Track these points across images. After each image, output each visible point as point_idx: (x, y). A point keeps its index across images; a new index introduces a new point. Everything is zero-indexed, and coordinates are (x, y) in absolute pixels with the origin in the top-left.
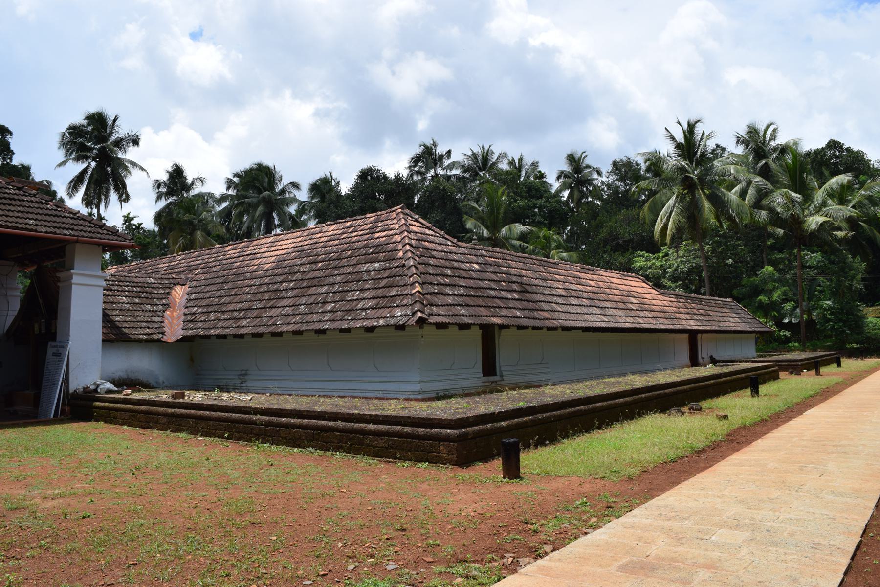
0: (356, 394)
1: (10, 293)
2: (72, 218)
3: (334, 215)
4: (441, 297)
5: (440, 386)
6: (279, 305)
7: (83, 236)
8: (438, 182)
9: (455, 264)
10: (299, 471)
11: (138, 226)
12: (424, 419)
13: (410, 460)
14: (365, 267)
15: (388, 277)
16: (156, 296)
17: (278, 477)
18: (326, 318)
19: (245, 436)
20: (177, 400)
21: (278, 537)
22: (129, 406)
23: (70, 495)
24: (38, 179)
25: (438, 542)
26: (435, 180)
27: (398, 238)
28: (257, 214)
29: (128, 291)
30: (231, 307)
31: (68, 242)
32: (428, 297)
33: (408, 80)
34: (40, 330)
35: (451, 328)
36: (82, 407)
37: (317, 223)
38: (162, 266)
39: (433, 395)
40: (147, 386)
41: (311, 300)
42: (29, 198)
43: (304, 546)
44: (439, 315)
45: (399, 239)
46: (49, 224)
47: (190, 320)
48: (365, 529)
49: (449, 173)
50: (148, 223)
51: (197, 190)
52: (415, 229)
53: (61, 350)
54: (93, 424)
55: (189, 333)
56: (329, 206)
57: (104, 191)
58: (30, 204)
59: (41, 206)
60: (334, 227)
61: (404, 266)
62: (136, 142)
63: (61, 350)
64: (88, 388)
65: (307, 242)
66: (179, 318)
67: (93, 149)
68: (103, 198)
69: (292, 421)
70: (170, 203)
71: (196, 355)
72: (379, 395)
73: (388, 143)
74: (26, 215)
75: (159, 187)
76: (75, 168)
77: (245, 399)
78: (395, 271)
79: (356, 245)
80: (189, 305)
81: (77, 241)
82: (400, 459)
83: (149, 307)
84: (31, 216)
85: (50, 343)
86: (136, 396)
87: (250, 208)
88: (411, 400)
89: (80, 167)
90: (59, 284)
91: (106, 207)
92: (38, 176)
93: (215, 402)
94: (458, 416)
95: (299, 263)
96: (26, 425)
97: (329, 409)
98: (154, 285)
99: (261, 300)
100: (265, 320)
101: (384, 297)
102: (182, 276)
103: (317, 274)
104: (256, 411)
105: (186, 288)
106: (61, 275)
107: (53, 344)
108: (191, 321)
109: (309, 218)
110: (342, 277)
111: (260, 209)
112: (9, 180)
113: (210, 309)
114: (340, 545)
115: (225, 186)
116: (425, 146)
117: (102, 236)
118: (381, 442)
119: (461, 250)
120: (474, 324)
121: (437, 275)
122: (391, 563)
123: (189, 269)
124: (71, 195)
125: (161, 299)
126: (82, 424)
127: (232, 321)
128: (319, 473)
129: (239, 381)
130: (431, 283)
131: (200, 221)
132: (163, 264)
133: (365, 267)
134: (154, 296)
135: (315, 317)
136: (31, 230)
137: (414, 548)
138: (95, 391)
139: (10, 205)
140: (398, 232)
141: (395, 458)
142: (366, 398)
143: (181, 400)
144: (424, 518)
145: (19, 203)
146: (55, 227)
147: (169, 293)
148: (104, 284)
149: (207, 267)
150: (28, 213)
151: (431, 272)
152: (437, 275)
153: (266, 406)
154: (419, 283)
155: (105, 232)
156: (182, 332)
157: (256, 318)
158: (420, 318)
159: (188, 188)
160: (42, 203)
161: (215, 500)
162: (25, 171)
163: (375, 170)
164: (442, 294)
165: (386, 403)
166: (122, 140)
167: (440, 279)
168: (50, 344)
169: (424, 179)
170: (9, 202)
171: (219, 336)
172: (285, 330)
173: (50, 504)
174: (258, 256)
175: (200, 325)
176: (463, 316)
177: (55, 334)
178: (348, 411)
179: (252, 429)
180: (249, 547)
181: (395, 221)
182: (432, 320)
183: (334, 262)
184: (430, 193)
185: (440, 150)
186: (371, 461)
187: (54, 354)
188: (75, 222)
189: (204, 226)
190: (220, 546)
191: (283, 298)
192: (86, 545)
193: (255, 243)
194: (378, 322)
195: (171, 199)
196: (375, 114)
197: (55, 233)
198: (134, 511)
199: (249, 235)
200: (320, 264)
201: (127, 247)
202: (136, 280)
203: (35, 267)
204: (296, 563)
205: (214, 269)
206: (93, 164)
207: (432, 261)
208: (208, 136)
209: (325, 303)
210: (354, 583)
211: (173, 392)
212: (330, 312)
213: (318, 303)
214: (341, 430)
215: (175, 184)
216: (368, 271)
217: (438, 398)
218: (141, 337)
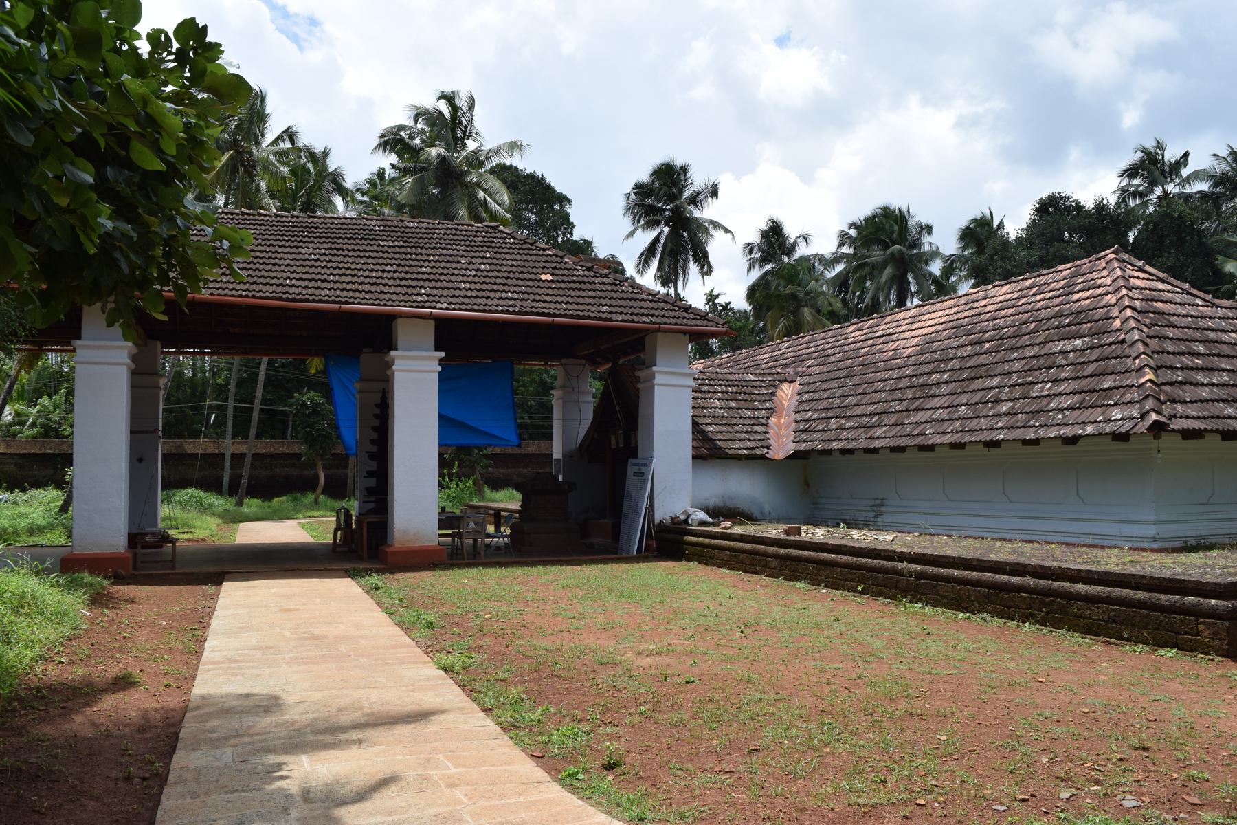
0: (1050, 539)
1: (582, 398)
3: (999, 271)
4: (1188, 388)
5: (1190, 530)
6: (928, 406)
8: (1168, 205)
9: (1212, 335)
10: (970, 646)
11: (726, 307)
12: (1169, 580)
13: (1146, 643)
14: (1059, 346)
15: (1097, 360)
16: (758, 398)
17: (940, 652)
18: (1000, 424)
19: (887, 591)
20: (792, 538)
21: (950, 737)
23: (668, 652)
24: (601, 256)
25: (1207, 776)
26: (1164, 203)
27: (1112, 299)
28: (884, 278)
30: (859, 411)
32: (1168, 388)
33: (1096, 55)
34: (617, 443)
35: (1208, 437)
36: (670, 542)
37: (975, 286)
39: (1178, 544)
40: (750, 518)
41: (977, 398)
42: (600, 280)
43: (989, 754)
44: (1187, 417)
45: (1113, 301)
46: (625, 311)
47: (804, 428)
48: (1082, 741)
49: (1188, 190)
50: (740, 302)
51: (802, 251)
52: (1138, 283)
53: (643, 469)
54: (684, 564)
55: (803, 446)
56: (992, 259)
57: (680, 264)
58: (602, 287)
60: (1005, 289)
61: (1123, 341)
62: (714, 192)
63: (643, 469)
65: (966, 314)
66: (788, 426)
67: (664, 210)
68: (680, 272)
69: (956, 573)
70: (766, 273)
71: (811, 476)
72: (1088, 542)
73: (1074, 153)
74: (598, 301)
76: (645, 238)
77: (884, 539)
78: (1108, 350)
79: (1043, 314)
80: (801, 408)
81: (659, 330)
82: (1128, 640)
83: (749, 413)
84: (604, 302)
86: (737, 530)
87: (873, 271)
88: (1144, 550)
89: (652, 234)
90: (639, 386)
91: (684, 283)
92: (601, 252)
93: (843, 542)
94: (1230, 579)
95: (955, 344)
96: (606, 561)
97: (1012, 558)
99: (901, 400)
100: (909, 428)
101: (1093, 391)
102: (790, 370)
103: (983, 359)
104: (902, 557)
105: (796, 387)
106: (641, 374)
108: (805, 431)
109: (960, 280)
110: (1023, 362)
111: (888, 271)
112: (576, 260)
113: (830, 414)
114: (1045, 760)
116: (1144, 151)
117: (689, 322)
118: (1097, 613)
119: (1221, 312)
120: (1211, 431)
121: (1180, 354)
122: (1129, 797)
123: (799, 360)
124: (640, 272)
126: (671, 564)
127: (861, 430)
128: (1000, 651)
129: (872, 514)
130: (1171, 368)
131: (807, 294)
132: (764, 354)
133: (1059, 346)
134: (753, 398)
135: (984, 424)
136: (606, 319)
137: (1166, 779)
138: (686, 521)
140: (1110, 289)
141: (1121, 638)
142: (1067, 544)
143: (797, 538)
144: (1179, 734)
145: (589, 286)
146: (632, 314)
147: (773, 394)
148: (694, 384)
149: (822, 357)
151: (1171, 349)
152: (1180, 354)
153: (916, 550)
154: (1151, 368)
155: (692, 316)
156: (793, 446)
157: (895, 425)
158: (1156, 422)
159: (790, 250)
161: (854, 676)
162: (587, 245)
163: (1061, 197)
164: (1191, 384)
165: (1101, 553)
166: (698, 194)
167: (1186, 360)
168: (631, 461)
169: (1145, 204)
171: (843, 452)
172: (938, 441)
173: (645, 662)
174: (894, 337)
175: (817, 436)
176: (1230, 417)
177: (636, 448)
178: (1042, 563)
179: (897, 581)
180: (907, 745)
181: (1105, 273)
182: (1177, 424)
183: (1010, 340)
184: (1155, 224)
185: (1171, 154)
186: (1081, 641)
187: (636, 474)
188: (655, 305)
189: (811, 299)
190: (869, 741)
191: (933, 396)
192: (693, 717)
193: (888, 319)
194: (1084, 429)
195: (768, 267)
196: (1053, 113)
197: (633, 321)
198: (749, 680)
199: (874, 309)
200: (987, 345)
201: (713, 335)
202: (731, 377)
203: (609, 365)
204: (979, 777)
205: (833, 358)
206: (666, 230)
207: (1170, 333)
208: (807, 176)
209: (997, 401)
210: (1071, 818)
211: (785, 526)
212: (1007, 414)
213: (987, 402)
214: (1033, 591)
216: (1064, 353)
217: (1187, 549)
218: (740, 452)
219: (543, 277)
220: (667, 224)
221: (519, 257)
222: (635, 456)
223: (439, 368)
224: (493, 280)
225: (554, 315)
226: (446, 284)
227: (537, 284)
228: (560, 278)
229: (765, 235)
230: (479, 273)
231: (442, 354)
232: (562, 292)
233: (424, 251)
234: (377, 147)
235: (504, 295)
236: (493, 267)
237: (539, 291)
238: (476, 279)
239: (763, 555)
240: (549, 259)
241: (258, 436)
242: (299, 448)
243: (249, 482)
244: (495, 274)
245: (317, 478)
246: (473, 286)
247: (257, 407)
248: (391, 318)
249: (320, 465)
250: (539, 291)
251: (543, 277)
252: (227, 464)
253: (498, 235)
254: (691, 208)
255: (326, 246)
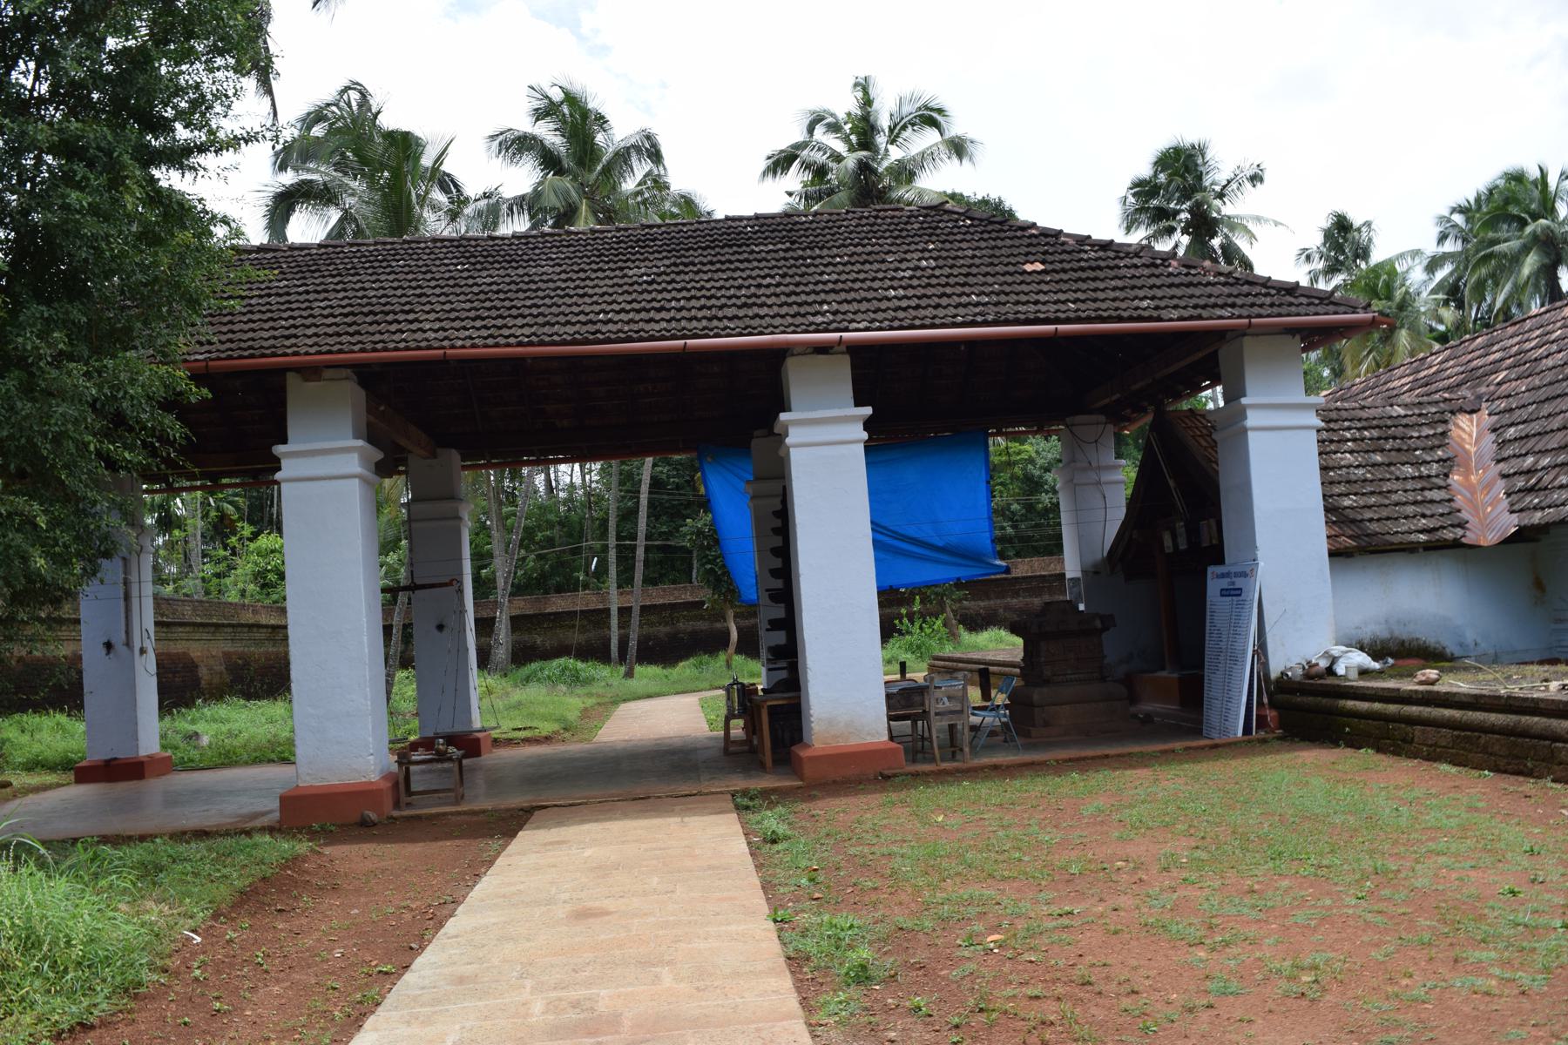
2: (1224, 284)
7: (1260, 316)
22: (1447, 713)
29: (1354, 440)
31: (1220, 335)
36: (1308, 712)
38: (1396, 383)
42: (1127, 261)
47: (1525, 487)
55: (1537, 517)
58: (1132, 271)
59: (1157, 272)
63: (1239, 583)
64: (1311, 665)
75: (1308, 258)
83: (1409, 470)
84: (1141, 293)
85: (1211, 570)
98: (1404, 421)
102: (1464, 391)
105: (1485, 418)
107: (1219, 569)
115: (1435, 232)
125: (1432, 448)
139: (1094, 279)
145: (1111, 273)
147: (1444, 434)
150: (1133, 287)
155: (1304, 300)
160: (1157, 266)
168: (1211, 570)
170: (1092, 274)
187: (1225, 593)
202: (1364, 414)
203: (1149, 419)
206: (1186, 240)
215: (1340, 249)
218: (1413, 537)
219: (1029, 267)
220: (1185, 231)
221: (983, 244)
222: (1220, 560)
223: (865, 436)
224: (943, 280)
225: (1057, 321)
226: (863, 294)
227: (1019, 278)
228: (1058, 266)
229: (1328, 235)
230: (919, 273)
231: (868, 411)
232: (1064, 287)
233: (825, 252)
234: (764, 174)
235: (964, 299)
236: (941, 262)
237: (1025, 288)
238: (915, 282)
239: (1541, 737)
240: (1034, 241)
241: (649, 581)
242: (705, 594)
243: (639, 642)
244: (947, 271)
245: (728, 633)
246: (910, 292)
247: (641, 542)
248: (776, 357)
249: (730, 614)
250: (1025, 288)
251: (1029, 267)
252: (614, 621)
253: (946, 217)
254: (1218, 202)
255: (667, 262)
